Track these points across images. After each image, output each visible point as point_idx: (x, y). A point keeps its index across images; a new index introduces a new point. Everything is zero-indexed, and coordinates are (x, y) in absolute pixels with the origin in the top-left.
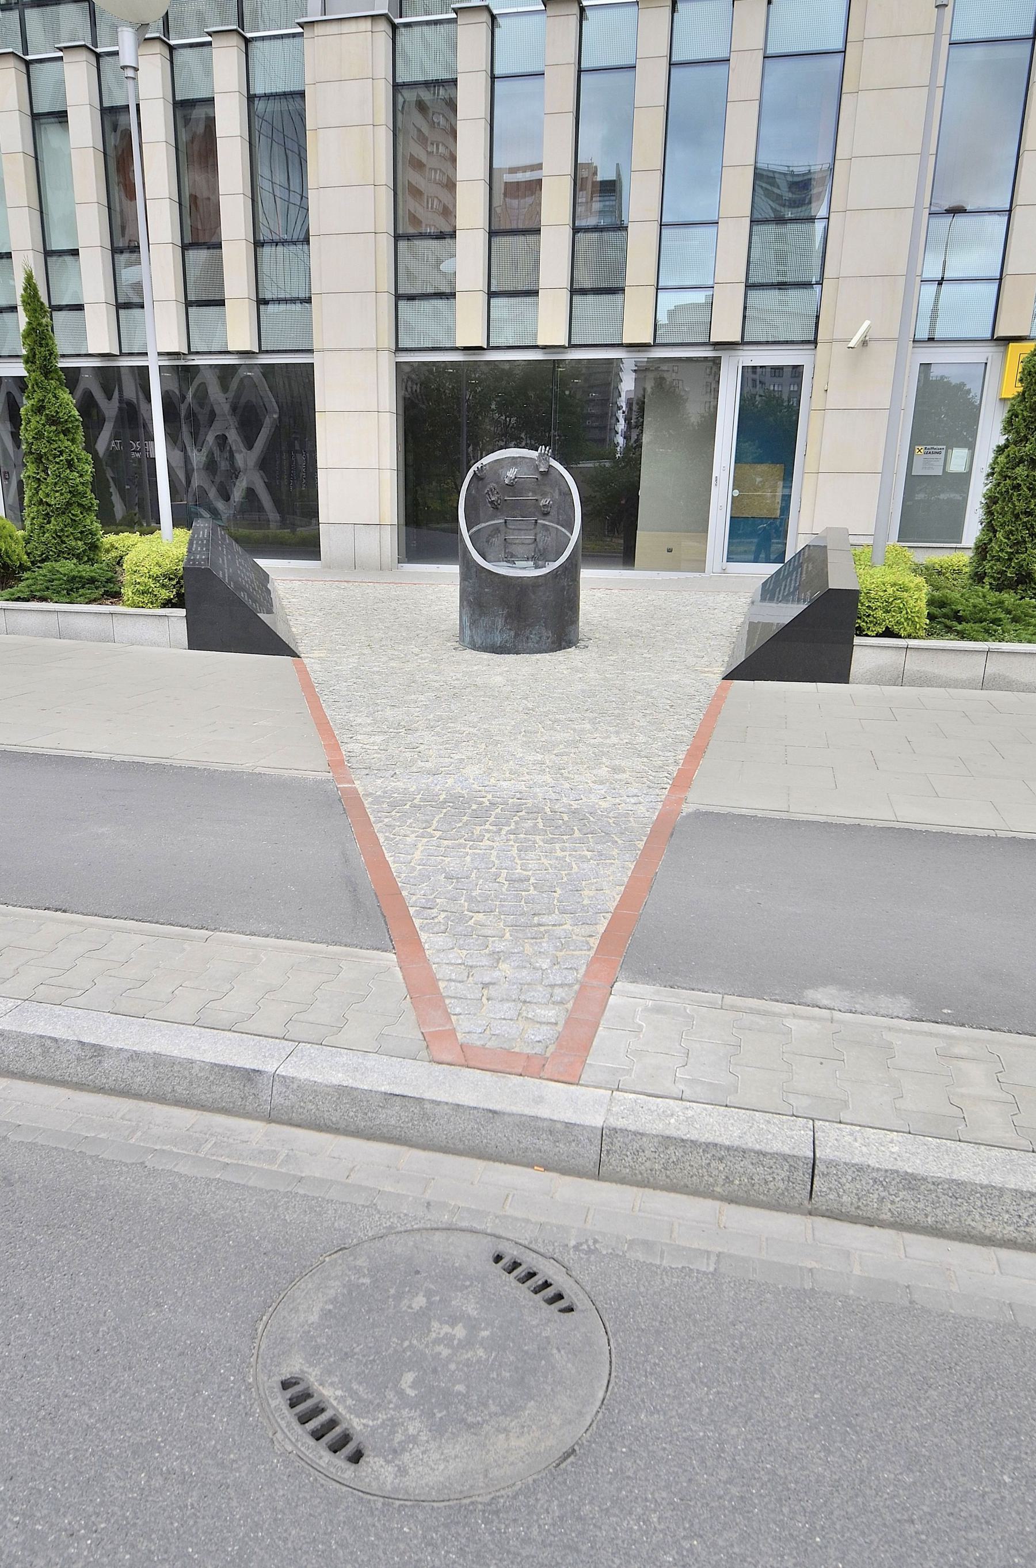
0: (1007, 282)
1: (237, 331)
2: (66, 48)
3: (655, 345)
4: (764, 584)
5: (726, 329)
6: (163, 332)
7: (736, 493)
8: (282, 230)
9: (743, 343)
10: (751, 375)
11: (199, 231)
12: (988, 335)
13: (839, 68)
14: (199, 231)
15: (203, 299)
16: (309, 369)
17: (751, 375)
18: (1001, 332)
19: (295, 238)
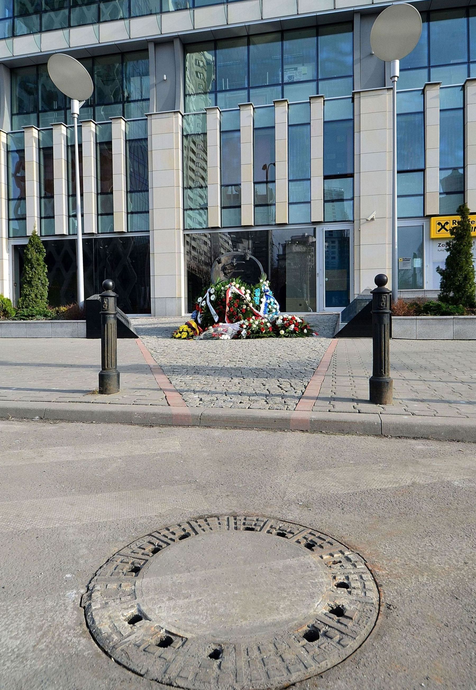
0: (427, 196)
1: (121, 223)
2: (54, 125)
3: (289, 224)
4: (447, 259)
5: (317, 216)
6: (91, 224)
7: (327, 279)
8: (139, 183)
9: (324, 222)
10: (329, 234)
11: (105, 190)
12: (422, 215)
13: (352, 125)
14: (105, 190)
15: (106, 211)
16: (147, 240)
17: (329, 234)
18: (428, 213)
19: (143, 189)
